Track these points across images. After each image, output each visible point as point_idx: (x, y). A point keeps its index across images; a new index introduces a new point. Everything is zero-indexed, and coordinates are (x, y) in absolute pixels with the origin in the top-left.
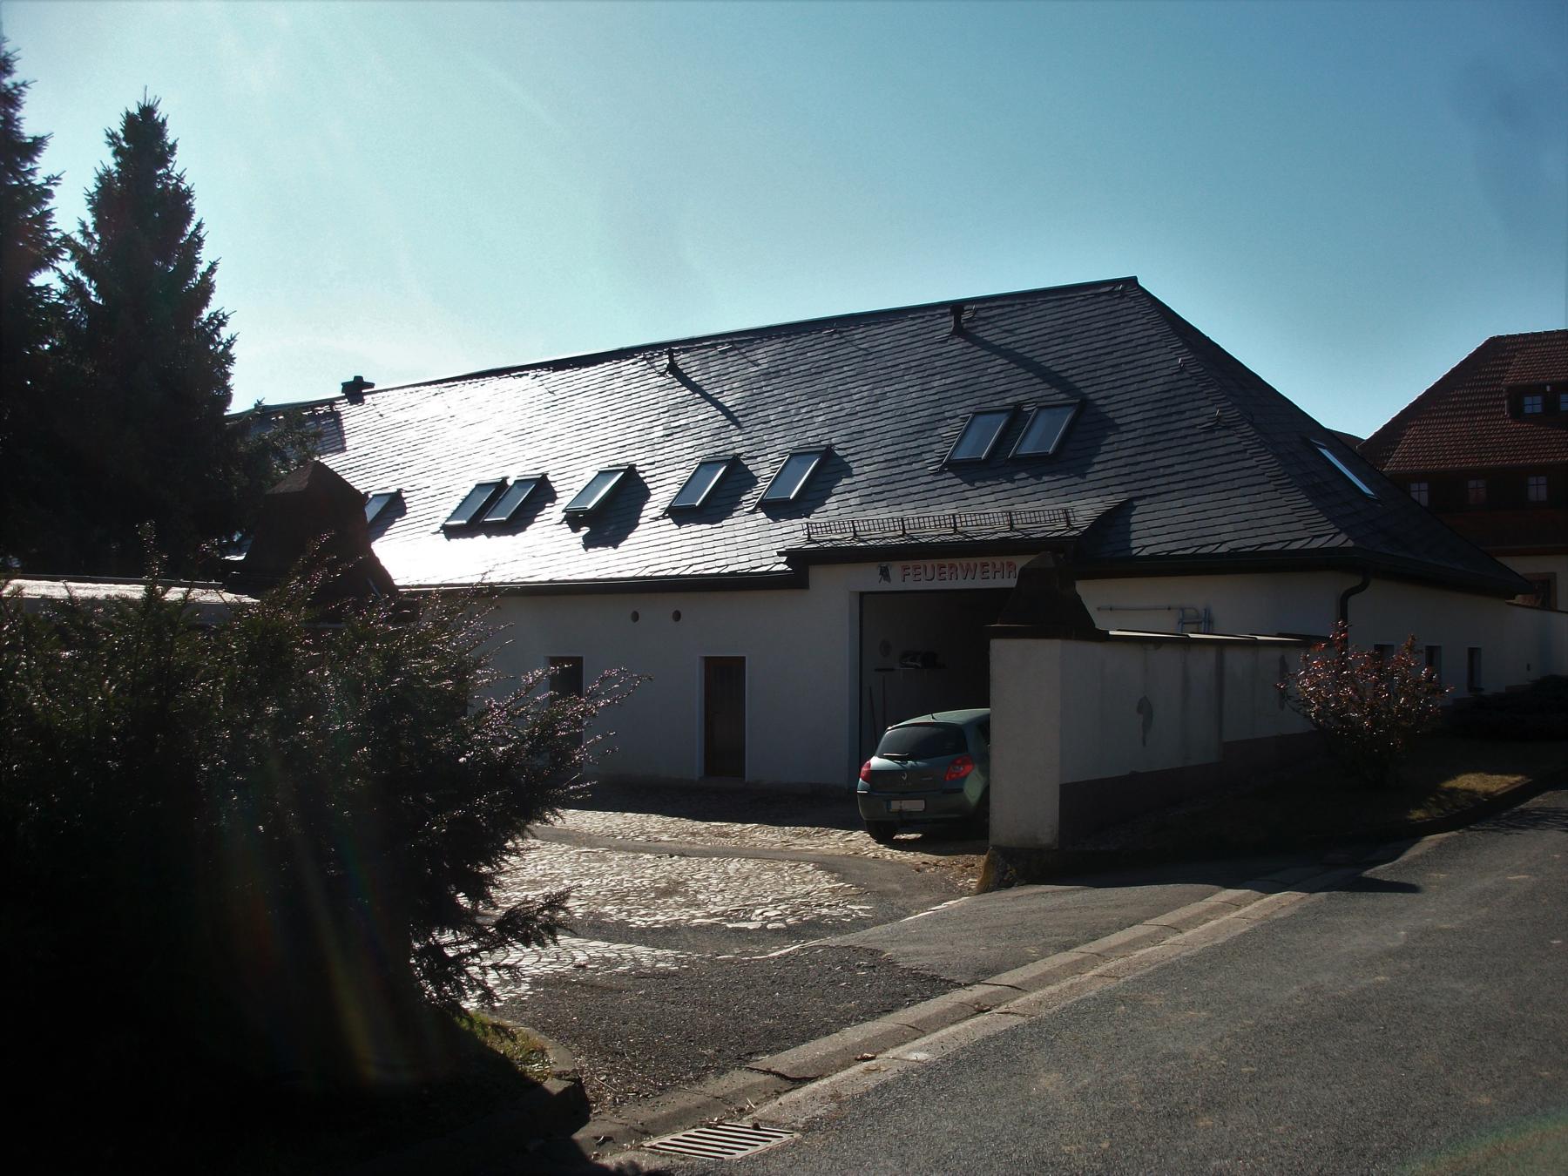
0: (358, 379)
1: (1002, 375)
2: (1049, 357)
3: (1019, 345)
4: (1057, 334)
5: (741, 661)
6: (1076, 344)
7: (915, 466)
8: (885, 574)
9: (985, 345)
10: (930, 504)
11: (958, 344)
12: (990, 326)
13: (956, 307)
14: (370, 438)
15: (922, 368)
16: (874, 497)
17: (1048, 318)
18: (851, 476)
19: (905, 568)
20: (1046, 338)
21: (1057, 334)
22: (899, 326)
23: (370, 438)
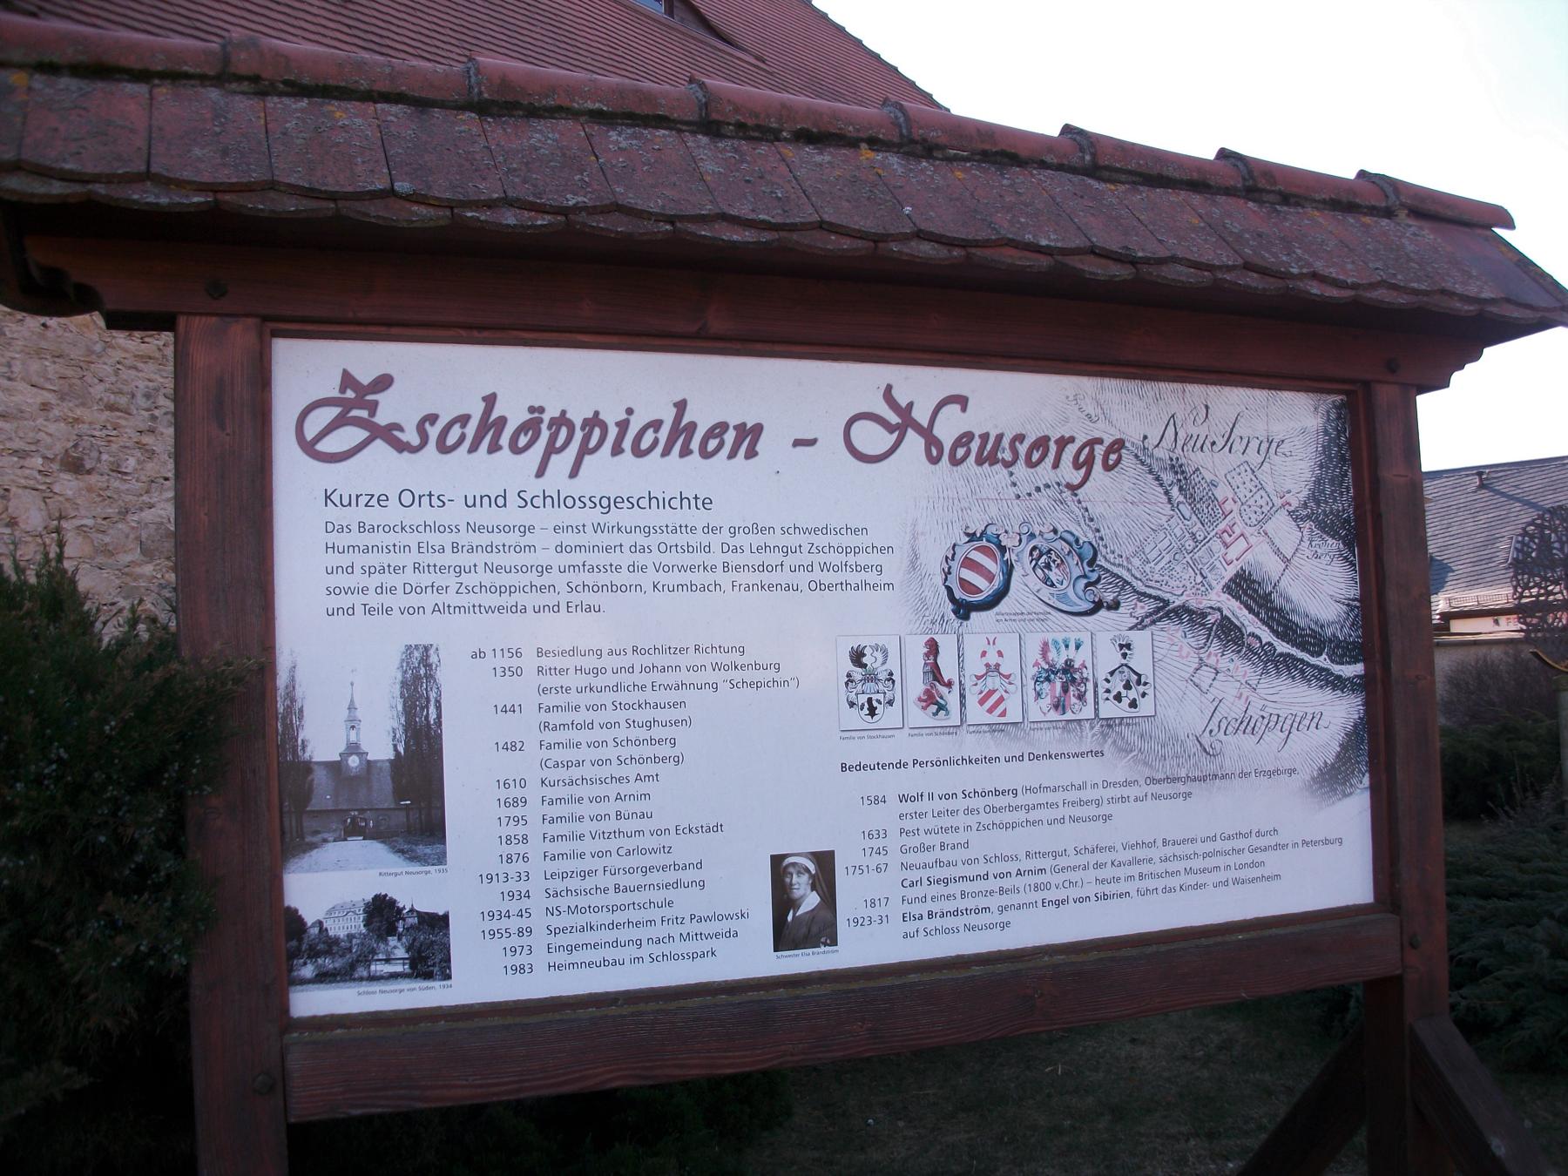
0: (751, 453)
1: (1522, 513)
2: (1548, 502)
3: (1525, 494)
4: (1548, 488)
5: (772, 856)
6: (1561, 494)
7: (1490, 565)
8: (1497, 622)
9: (1503, 494)
10: (622, 939)
11: (1485, 494)
12: (1501, 483)
13: (1479, 471)
14: (947, 821)
15: (1468, 508)
16: (1472, 583)
17: (1537, 478)
18: (1453, 571)
19: (1508, 619)
20: (1541, 490)
21: (1548, 488)
22: (1438, 482)
23: (947, 821)
